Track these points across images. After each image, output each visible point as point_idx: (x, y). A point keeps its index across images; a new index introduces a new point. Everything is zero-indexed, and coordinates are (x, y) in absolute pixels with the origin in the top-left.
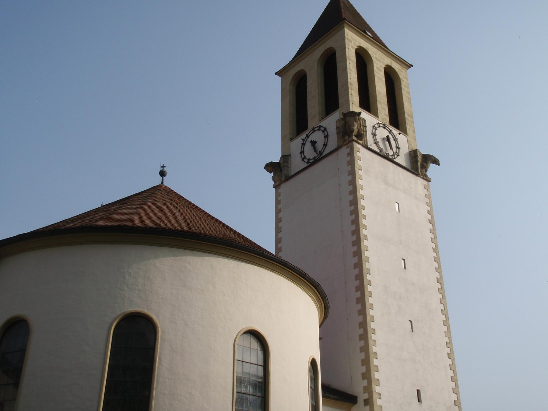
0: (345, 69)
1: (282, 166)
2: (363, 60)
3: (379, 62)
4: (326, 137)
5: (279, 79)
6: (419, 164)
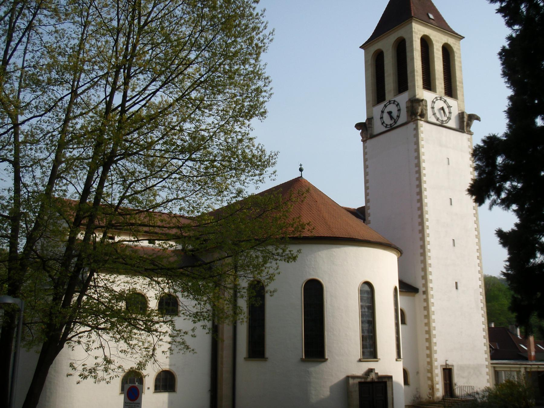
0: (412, 59)
1: (368, 126)
2: (426, 42)
3: (438, 40)
4: (399, 110)
5: (363, 51)
6: (465, 123)
